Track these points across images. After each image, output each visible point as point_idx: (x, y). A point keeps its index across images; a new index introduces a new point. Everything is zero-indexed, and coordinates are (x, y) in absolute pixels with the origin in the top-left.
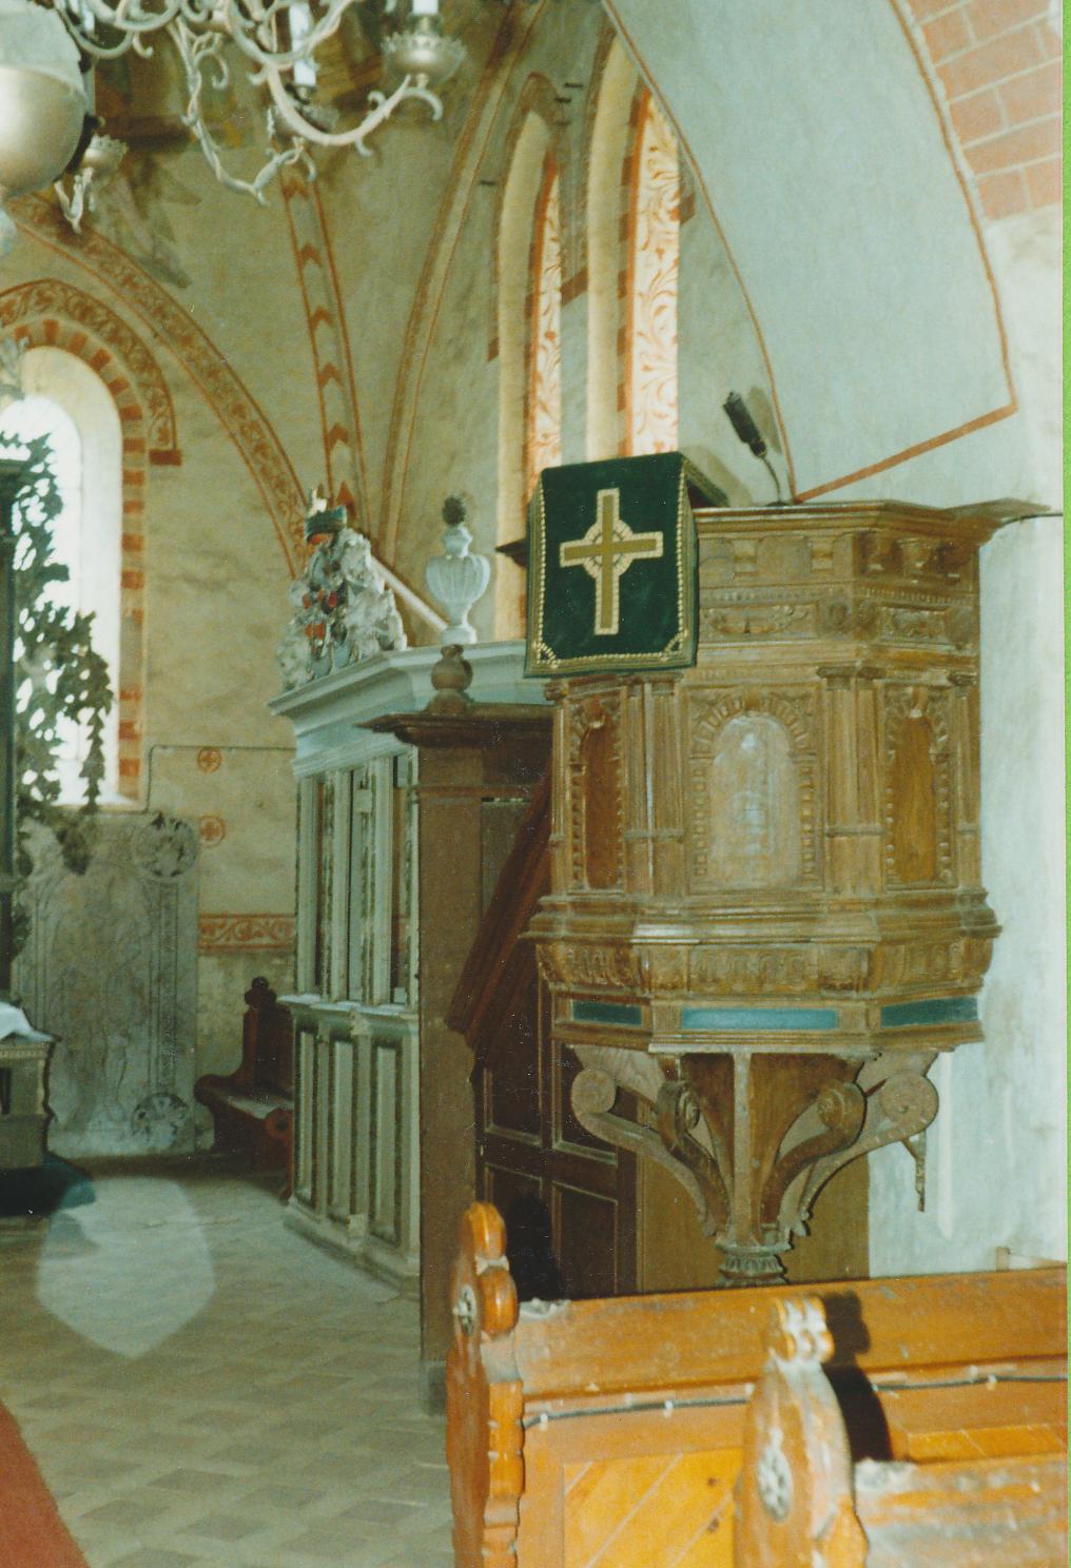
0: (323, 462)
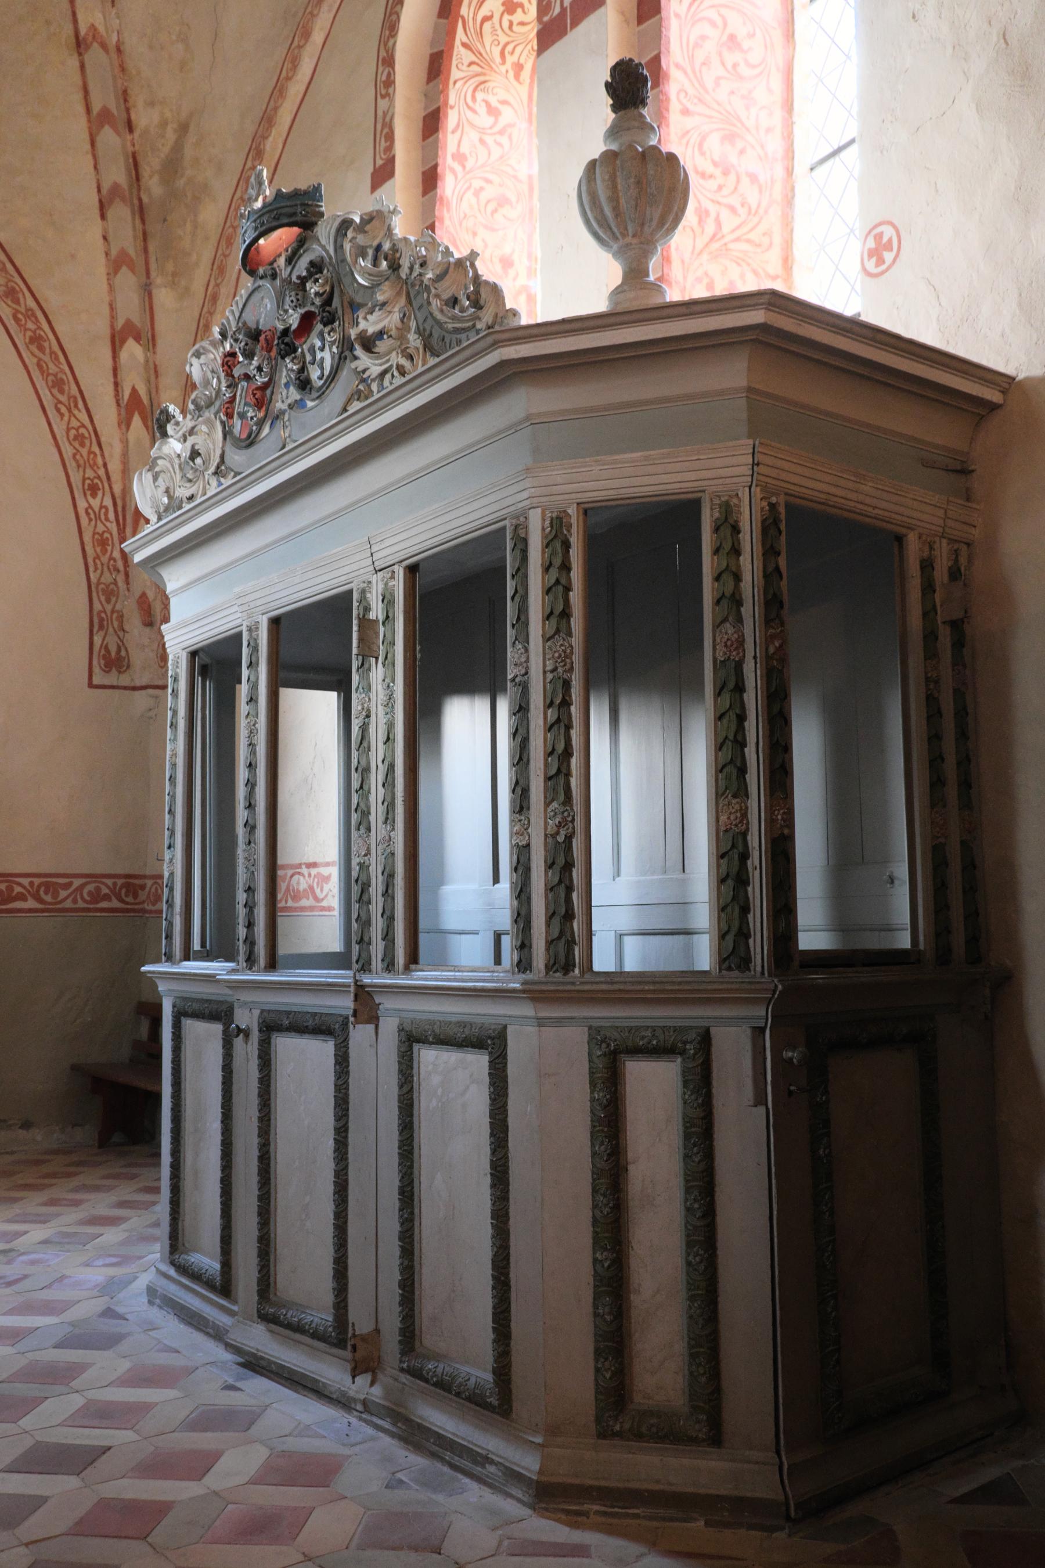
0: (109, 363)
